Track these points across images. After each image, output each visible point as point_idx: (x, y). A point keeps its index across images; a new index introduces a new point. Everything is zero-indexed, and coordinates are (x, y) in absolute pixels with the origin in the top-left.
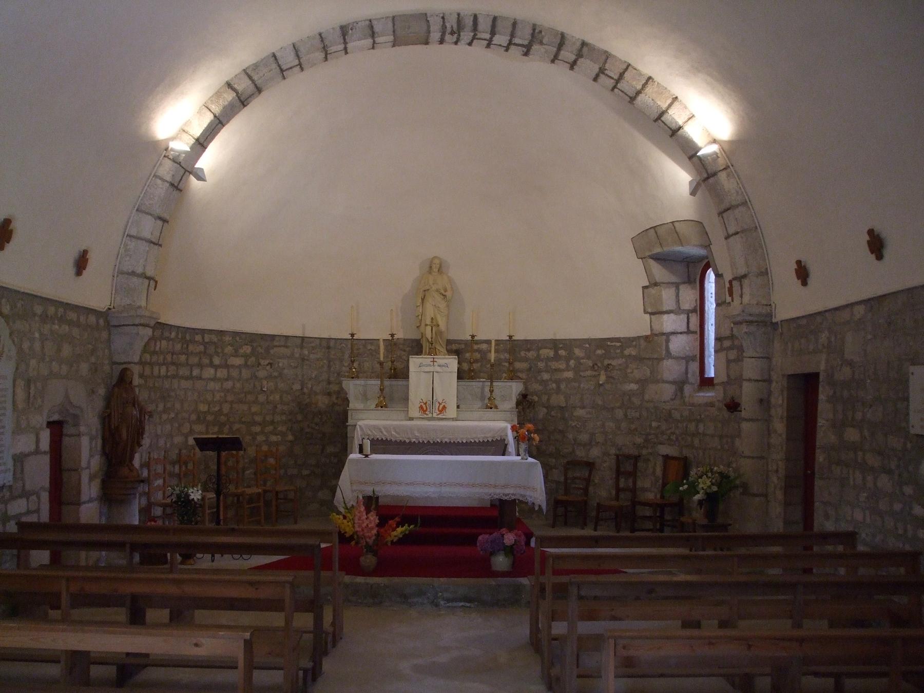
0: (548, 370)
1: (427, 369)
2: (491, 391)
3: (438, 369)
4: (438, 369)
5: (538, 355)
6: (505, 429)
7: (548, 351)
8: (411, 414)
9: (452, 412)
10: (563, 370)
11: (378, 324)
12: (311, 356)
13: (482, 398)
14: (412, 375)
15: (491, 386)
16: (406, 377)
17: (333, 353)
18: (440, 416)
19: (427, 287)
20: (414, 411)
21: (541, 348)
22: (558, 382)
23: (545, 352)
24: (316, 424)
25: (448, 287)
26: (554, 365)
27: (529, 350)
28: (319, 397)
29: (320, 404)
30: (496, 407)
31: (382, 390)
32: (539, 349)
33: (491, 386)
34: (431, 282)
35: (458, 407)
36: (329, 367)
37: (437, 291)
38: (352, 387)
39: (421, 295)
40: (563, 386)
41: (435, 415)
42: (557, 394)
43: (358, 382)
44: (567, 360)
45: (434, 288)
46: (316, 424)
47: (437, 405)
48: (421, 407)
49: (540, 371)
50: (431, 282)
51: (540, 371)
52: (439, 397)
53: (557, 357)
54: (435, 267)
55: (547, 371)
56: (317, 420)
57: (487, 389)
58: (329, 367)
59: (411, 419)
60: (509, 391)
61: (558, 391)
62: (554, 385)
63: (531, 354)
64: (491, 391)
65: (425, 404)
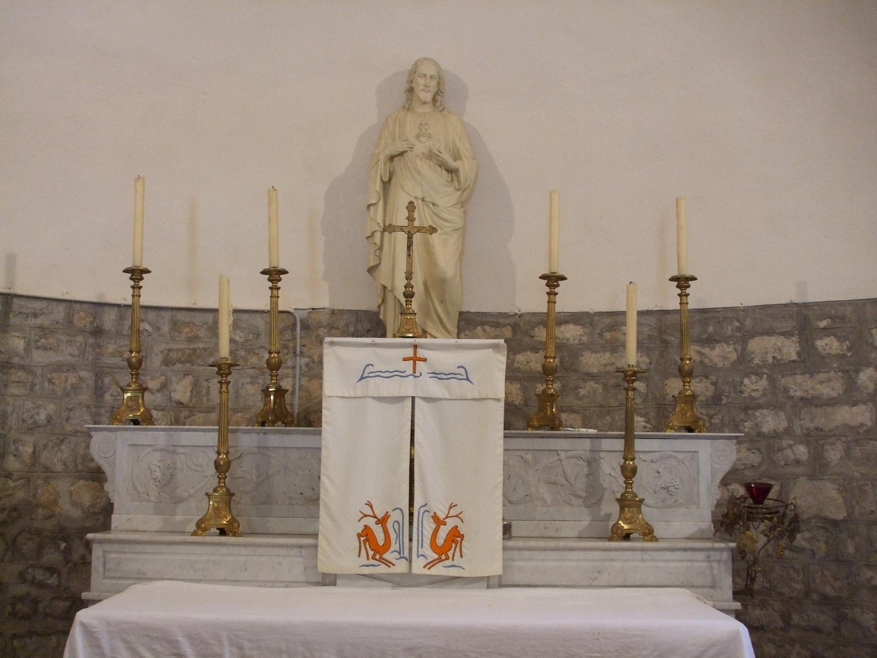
0: (777, 400)
1: (391, 387)
2: (629, 473)
3: (435, 388)
4: (435, 388)
5: (744, 358)
6: (734, 638)
7: (778, 341)
8: (327, 563)
9: (484, 552)
10: (832, 402)
11: (220, 242)
12: (38, 357)
13: (593, 495)
14: (333, 414)
15: (629, 451)
16: (310, 418)
17: (111, 348)
18: (439, 570)
19: (400, 147)
20: (339, 549)
21: (753, 334)
22: (816, 439)
23: (762, 347)
24: (51, 570)
25: (464, 149)
26: (800, 385)
27: (711, 341)
28: (62, 486)
29: (65, 506)
30: (648, 534)
31: (222, 468)
32: (744, 336)
33: (629, 451)
34: (411, 131)
35: (507, 529)
36: (99, 391)
37: (431, 156)
38: (126, 455)
39: (381, 171)
40: (834, 454)
41: (418, 566)
42: (812, 477)
43: (143, 436)
44: (849, 368)
45: (420, 148)
46: (51, 570)
47: (429, 527)
48: (366, 535)
49: (750, 407)
50: (411, 131)
51: (750, 407)
52: (434, 494)
53: (810, 362)
54: (425, 92)
55: (775, 407)
56: (51, 556)
57: (610, 467)
58: (99, 391)
59: (329, 580)
60: (692, 470)
61: (817, 467)
62: (801, 451)
63: (721, 354)
64: (629, 473)
65: (382, 521)
